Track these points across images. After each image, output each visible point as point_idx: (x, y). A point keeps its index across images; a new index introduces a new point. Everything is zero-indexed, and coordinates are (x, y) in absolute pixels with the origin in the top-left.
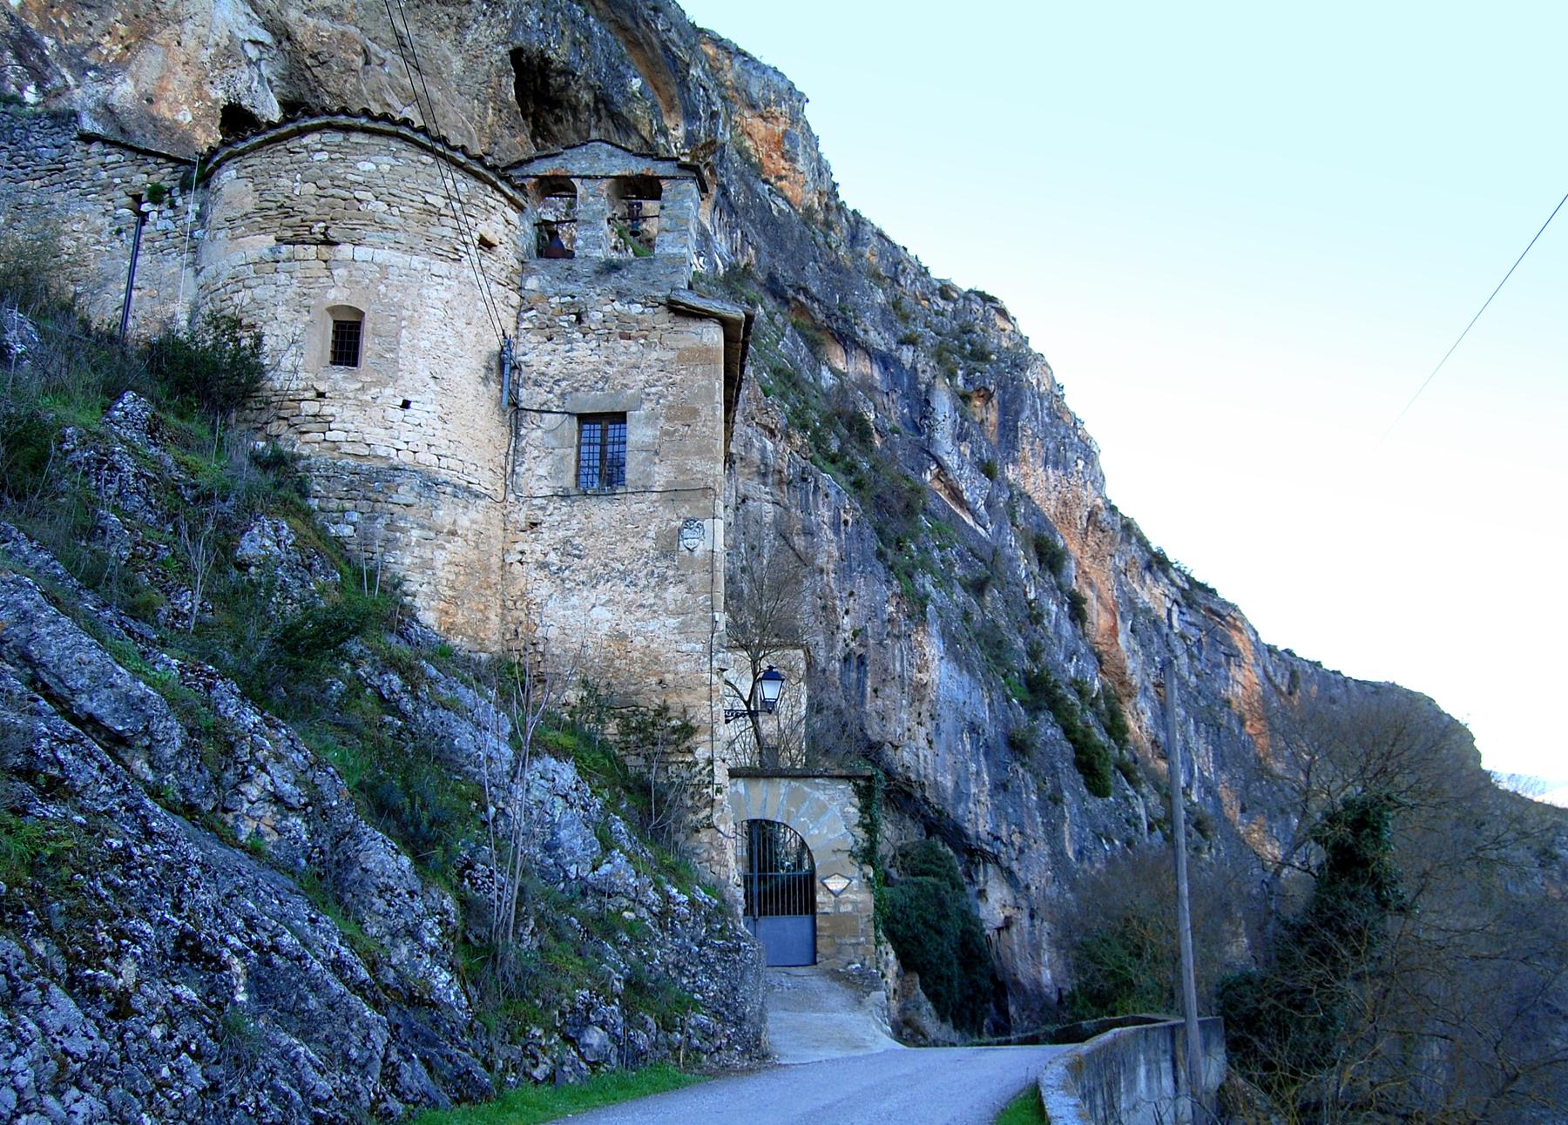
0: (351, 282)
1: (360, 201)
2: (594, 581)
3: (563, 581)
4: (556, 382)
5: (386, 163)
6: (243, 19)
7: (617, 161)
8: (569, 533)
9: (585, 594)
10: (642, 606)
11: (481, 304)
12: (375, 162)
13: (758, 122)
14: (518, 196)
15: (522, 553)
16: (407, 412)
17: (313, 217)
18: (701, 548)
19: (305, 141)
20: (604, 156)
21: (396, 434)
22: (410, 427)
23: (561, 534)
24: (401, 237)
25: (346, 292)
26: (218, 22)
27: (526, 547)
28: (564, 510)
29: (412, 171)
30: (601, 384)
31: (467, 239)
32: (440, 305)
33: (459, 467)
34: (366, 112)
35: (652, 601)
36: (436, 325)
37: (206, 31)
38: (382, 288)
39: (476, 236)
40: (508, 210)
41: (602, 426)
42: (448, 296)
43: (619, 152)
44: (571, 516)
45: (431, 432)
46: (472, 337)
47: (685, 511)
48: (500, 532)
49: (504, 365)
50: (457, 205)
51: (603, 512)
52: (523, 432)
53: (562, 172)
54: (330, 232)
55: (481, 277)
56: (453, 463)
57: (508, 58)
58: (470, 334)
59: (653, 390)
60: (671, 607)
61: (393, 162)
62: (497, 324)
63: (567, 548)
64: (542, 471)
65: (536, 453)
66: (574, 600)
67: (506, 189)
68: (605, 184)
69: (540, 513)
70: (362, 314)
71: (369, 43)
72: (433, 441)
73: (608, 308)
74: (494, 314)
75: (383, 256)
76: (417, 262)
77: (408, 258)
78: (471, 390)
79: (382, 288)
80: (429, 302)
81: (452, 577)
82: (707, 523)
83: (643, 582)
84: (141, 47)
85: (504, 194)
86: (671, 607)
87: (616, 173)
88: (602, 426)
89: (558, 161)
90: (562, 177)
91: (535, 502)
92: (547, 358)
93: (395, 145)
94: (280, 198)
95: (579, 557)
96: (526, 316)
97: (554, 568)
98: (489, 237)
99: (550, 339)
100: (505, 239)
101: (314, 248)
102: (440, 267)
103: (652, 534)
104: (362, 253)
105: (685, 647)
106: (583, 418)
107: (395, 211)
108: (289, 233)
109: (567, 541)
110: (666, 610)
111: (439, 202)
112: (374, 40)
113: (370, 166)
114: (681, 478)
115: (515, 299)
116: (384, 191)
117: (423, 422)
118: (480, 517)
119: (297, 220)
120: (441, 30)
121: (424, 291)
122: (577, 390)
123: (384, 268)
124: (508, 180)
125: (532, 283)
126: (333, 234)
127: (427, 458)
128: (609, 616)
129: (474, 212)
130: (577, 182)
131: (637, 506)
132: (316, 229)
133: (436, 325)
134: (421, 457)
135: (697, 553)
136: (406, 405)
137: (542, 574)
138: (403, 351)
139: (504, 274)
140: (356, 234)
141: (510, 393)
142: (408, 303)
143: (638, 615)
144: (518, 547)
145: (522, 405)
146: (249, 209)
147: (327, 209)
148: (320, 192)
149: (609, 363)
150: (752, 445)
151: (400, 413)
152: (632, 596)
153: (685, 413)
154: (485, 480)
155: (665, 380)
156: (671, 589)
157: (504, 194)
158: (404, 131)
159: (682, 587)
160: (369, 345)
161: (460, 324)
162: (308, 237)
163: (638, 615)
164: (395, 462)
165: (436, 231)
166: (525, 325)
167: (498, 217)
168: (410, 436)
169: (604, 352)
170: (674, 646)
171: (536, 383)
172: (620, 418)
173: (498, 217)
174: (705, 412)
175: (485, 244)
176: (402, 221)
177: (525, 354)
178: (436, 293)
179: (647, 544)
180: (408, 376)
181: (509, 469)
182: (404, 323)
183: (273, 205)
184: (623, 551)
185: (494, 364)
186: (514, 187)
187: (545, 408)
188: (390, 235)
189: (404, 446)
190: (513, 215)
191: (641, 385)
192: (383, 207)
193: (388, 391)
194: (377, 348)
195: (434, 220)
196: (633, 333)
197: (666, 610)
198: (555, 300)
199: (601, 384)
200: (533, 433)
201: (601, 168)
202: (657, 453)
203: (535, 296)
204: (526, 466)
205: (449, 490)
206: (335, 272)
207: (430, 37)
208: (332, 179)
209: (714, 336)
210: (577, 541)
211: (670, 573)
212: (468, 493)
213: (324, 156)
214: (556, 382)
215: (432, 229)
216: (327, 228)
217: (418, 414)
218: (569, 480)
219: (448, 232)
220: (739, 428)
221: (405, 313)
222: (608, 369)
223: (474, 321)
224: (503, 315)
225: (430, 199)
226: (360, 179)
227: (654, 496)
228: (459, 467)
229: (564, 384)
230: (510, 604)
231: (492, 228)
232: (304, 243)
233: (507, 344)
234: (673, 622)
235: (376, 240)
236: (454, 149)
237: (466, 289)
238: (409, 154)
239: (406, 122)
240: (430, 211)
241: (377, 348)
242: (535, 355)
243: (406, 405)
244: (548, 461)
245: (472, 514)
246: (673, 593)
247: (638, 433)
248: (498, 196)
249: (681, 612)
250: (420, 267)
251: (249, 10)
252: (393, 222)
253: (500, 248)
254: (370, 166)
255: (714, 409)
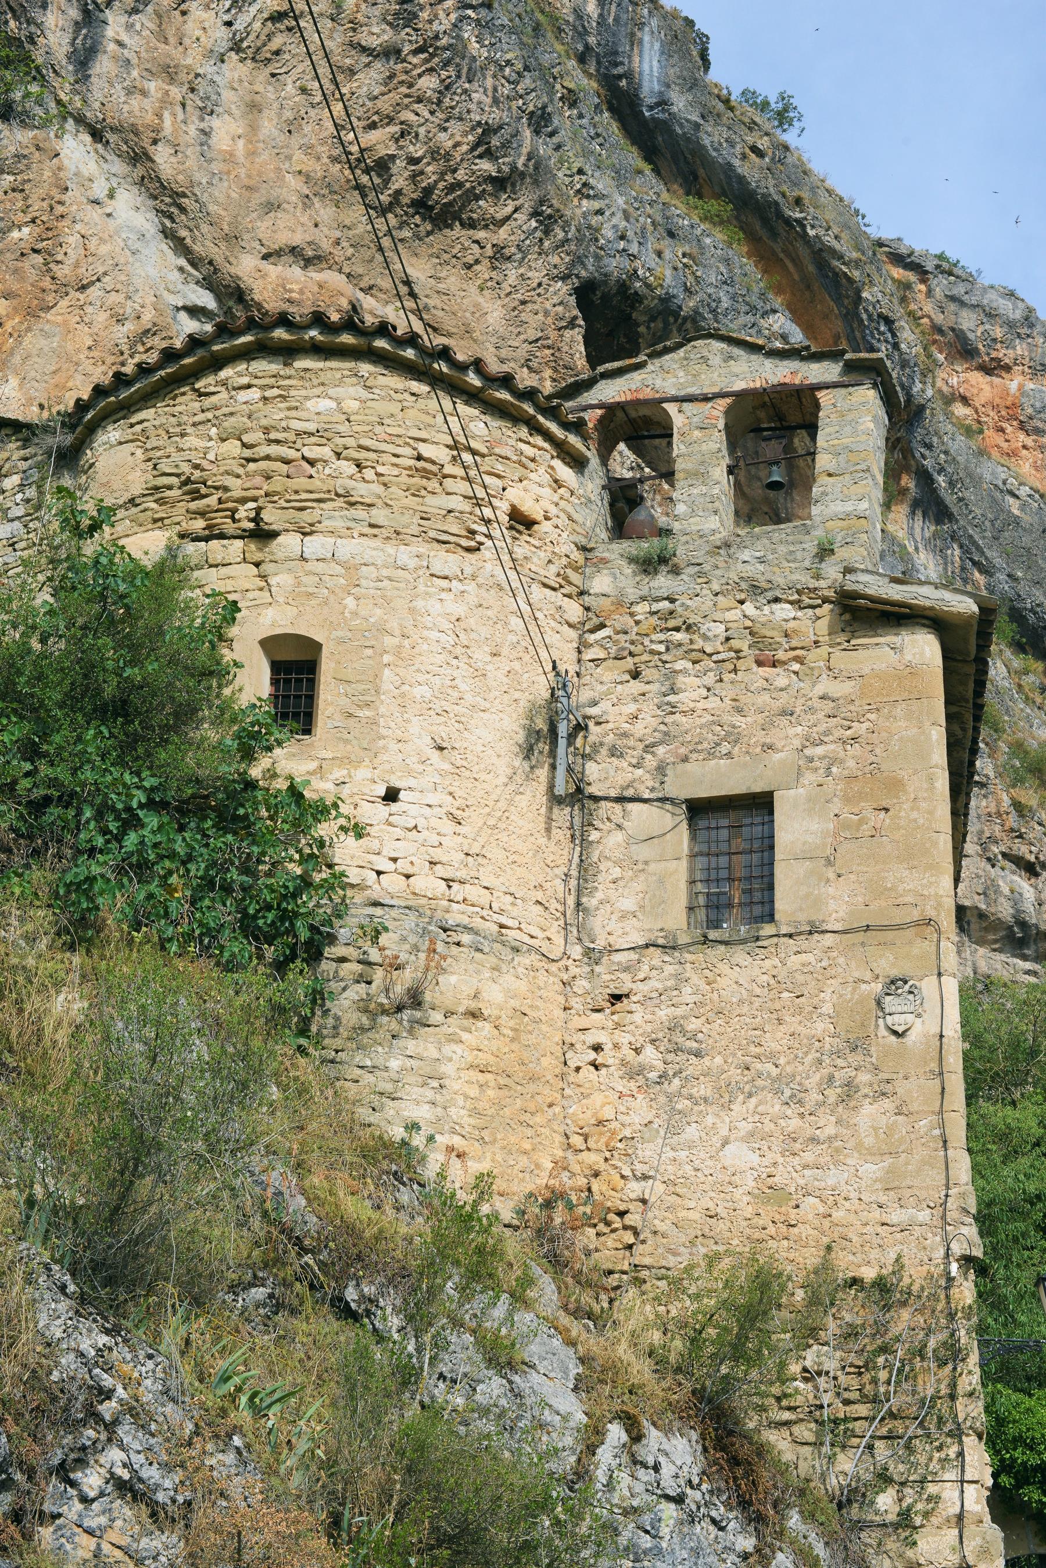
0: (299, 596)
1: (312, 463)
2: (725, 1096)
3: (670, 1097)
4: (649, 748)
5: (351, 396)
6: (176, 275)
7: (735, 367)
8: (679, 1012)
9: (710, 1120)
10: (814, 1140)
11: (516, 622)
12: (337, 395)
13: (977, 378)
14: (573, 439)
15: (597, 1048)
16: (394, 807)
17: (237, 494)
18: (921, 1030)
19: (223, 374)
20: (716, 360)
21: (375, 845)
22: (398, 832)
23: (664, 1013)
24: (379, 515)
25: (291, 611)
26: (138, 282)
27: (602, 1037)
28: (669, 969)
29: (395, 407)
30: (725, 748)
31: (488, 512)
32: (446, 626)
33: (485, 897)
34: (319, 319)
35: (830, 1130)
36: (440, 659)
37: (120, 298)
38: (350, 602)
39: (503, 506)
40: (557, 463)
41: (733, 832)
42: (460, 610)
43: (737, 351)
44: (681, 980)
45: (434, 839)
46: (500, 675)
47: (887, 965)
48: (558, 1013)
49: (555, 731)
50: (467, 457)
51: (740, 971)
52: (594, 836)
53: (647, 394)
54: (265, 515)
55: (512, 575)
56: (472, 892)
57: (572, 300)
58: (497, 672)
59: (820, 750)
60: (869, 1141)
61: (364, 394)
62: (544, 654)
63: (676, 1041)
64: (628, 904)
65: (617, 872)
66: (692, 1132)
67: (553, 427)
68: (717, 411)
69: (625, 977)
70: (317, 647)
71: (360, 295)
72: (438, 854)
73: (734, 615)
74: (537, 639)
75: (348, 548)
76: (405, 555)
77: (390, 550)
78: (503, 769)
79: (350, 602)
80: (428, 621)
81: (474, 1091)
82: (928, 986)
83: (815, 1096)
84: (29, 329)
85: (548, 436)
86: (869, 1141)
87: (739, 386)
88: (733, 832)
89: (637, 376)
90: (646, 402)
91: (617, 957)
92: (632, 708)
93: (366, 368)
94: (186, 468)
95: (698, 1054)
96: (591, 638)
97: (653, 1075)
98: (530, 508)
99: (635, 675)
100: (553, 511)
101: (239, 543)
102: (446, 561)
103: (827, 1009)
104: (315, 545)
105: (896, 1216)
106: (698, 810)
107: (369, 474)
108: (199, 524)
109: (674, 1026)
110: (859, 1147)
111: (441, 454)
112: (368, 290)
113: (325, 404)
114: (874, 906)
115: (574, 610)
116: (351, 442)
117: (422, 823)
118: (522, 986)
119: (212, 501)
120: (469, 267)
121: (419, 603)
122: (685, 759)
123: (351, 568)
124: (553, 413)
125: (601, 583)
126: (271, 517)
127: (428, 883)
128: (754, 1159)
129: (499, 468)
130: (671, 408)
131: (797, 959)
132: (241, 514)
133: (440, 659)
134: (419, 883)
135: (912, 1037)
136: (391, 796)
137: (632, 1085)
138: (386, 706)
139: (553, 569)
140: (306, 517)
141: (570, 769)
142: (393, 625)
143: (808, 1157)
144: (591, 1038)
145: (594, 790)
146: (137, 490)
147: (258, 480)
148: (247, 453)
149: (739, 711)
150: (997, 891)
151: (382, 810)
152: (795, 1123)
153: (880, 789)
154: (533, 923)
155: (839, 733)
156: (868, 1110)
157: (548, 436)
158: (380, 343)
159: (887, 1104)
160: (330, 697)
161: (480, 655)
162: (229, 527)
163: (808, 1157)
164: (375, 894)
165: (436, 503)
166: (589, 654)
167: (541, 475)
168: (400, 849)
169: (727, 691)
170: (876, 1214)
171: (614, 752)
172: (761, 804)
173: (541, 475)
174: (914, 785)
175: (521, 521)
176: (379, 489)
177: (595, 703)
178: (440, 607)
179: (821, 1027)
180: (394, 746)
181: (571, 901)
182: (386, 659)
183: (174, 481)
184: (775, 1040)
185: (541, 724)
186: (566, 426)
187: (630, 793)
188: (360, 513)
189: (389, 866)
190: (565, 472)
191: (797, 743)
192: (349, 468)
193: (362, 773)
194: (344, 701)
195: (433, 485)
196: (781, 655)
197: (859, 1147)
198: (641, 609)
199: (725, 748)
200: (609, 841)
201: (712, 380)
202: (829, 863)
203: (605, 603)
204: (599, 895)
205: (466, 938)
206: (273, 581)
207: (453, 279)
208: (266, 430)
209: (924, 648)
210: (693, 1025)
211: (864, 1077)
212: (504, 943)
213: (254, 394)
214: (649, 748)
215: (430, 499)
216: (258, 510)
217: (413, 810)
218: (675, 917)
219: (456, 503)
220: (972, 866)
221: (389, 641)
222: (738, 720)
223: (505, 651)
224: (551, 638)
225: (426, 450)
226: (311, 427)
227: (829, 940)
228: (485, 897)
229: (661, 750)
230: (577, 1141)
231: (532, 494)
232: (222, 536)
233: (560, 687)
234: (871, 1170)
235: (339, 524)
236: (463, 367)
237: (490, 597)
238: (394, 381)
239: (384, 329)
240: (425, 469)
241: (344, 701)
242: (615, 703)
243: (391, 796)
244: (637, 886)
245: (508, 979)
246: (870, 1114)
247: (794, 829)
248: (539, 440)
249: (888, 1148)
250: (412, 563)
251: (182, 262)
252: (362, 491)
253: (546, 526)
254: (325, 404)
255: (931, 779)
